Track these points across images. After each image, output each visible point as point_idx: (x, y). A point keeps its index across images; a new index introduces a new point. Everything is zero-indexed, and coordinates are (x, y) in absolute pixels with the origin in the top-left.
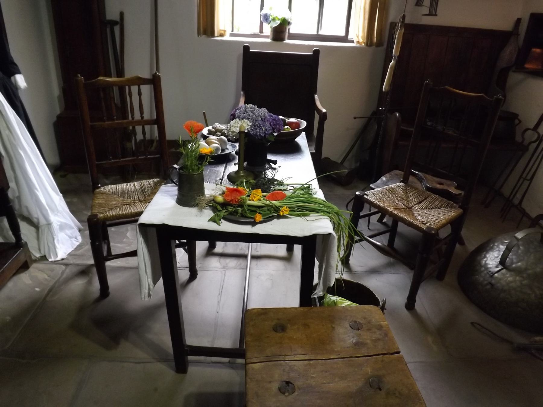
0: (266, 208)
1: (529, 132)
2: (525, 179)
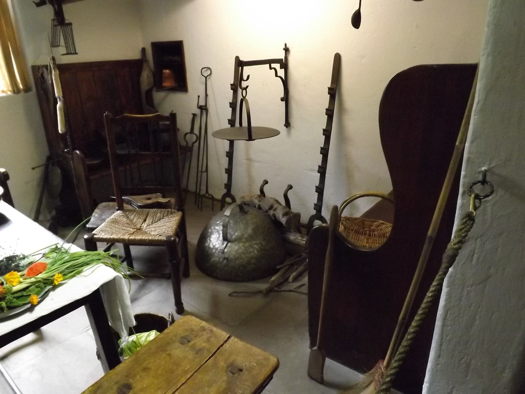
0: (33, 287)
1: (188, 136)
2: (202, 172)
